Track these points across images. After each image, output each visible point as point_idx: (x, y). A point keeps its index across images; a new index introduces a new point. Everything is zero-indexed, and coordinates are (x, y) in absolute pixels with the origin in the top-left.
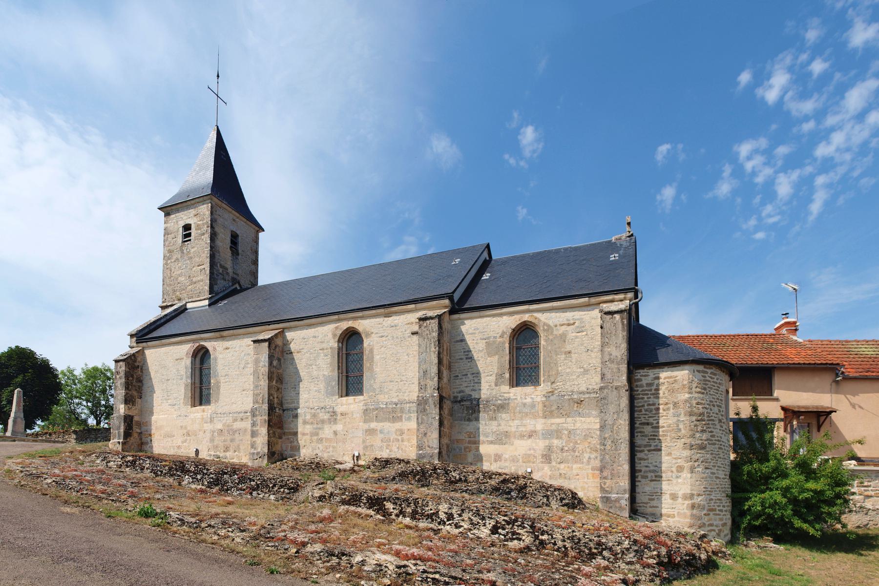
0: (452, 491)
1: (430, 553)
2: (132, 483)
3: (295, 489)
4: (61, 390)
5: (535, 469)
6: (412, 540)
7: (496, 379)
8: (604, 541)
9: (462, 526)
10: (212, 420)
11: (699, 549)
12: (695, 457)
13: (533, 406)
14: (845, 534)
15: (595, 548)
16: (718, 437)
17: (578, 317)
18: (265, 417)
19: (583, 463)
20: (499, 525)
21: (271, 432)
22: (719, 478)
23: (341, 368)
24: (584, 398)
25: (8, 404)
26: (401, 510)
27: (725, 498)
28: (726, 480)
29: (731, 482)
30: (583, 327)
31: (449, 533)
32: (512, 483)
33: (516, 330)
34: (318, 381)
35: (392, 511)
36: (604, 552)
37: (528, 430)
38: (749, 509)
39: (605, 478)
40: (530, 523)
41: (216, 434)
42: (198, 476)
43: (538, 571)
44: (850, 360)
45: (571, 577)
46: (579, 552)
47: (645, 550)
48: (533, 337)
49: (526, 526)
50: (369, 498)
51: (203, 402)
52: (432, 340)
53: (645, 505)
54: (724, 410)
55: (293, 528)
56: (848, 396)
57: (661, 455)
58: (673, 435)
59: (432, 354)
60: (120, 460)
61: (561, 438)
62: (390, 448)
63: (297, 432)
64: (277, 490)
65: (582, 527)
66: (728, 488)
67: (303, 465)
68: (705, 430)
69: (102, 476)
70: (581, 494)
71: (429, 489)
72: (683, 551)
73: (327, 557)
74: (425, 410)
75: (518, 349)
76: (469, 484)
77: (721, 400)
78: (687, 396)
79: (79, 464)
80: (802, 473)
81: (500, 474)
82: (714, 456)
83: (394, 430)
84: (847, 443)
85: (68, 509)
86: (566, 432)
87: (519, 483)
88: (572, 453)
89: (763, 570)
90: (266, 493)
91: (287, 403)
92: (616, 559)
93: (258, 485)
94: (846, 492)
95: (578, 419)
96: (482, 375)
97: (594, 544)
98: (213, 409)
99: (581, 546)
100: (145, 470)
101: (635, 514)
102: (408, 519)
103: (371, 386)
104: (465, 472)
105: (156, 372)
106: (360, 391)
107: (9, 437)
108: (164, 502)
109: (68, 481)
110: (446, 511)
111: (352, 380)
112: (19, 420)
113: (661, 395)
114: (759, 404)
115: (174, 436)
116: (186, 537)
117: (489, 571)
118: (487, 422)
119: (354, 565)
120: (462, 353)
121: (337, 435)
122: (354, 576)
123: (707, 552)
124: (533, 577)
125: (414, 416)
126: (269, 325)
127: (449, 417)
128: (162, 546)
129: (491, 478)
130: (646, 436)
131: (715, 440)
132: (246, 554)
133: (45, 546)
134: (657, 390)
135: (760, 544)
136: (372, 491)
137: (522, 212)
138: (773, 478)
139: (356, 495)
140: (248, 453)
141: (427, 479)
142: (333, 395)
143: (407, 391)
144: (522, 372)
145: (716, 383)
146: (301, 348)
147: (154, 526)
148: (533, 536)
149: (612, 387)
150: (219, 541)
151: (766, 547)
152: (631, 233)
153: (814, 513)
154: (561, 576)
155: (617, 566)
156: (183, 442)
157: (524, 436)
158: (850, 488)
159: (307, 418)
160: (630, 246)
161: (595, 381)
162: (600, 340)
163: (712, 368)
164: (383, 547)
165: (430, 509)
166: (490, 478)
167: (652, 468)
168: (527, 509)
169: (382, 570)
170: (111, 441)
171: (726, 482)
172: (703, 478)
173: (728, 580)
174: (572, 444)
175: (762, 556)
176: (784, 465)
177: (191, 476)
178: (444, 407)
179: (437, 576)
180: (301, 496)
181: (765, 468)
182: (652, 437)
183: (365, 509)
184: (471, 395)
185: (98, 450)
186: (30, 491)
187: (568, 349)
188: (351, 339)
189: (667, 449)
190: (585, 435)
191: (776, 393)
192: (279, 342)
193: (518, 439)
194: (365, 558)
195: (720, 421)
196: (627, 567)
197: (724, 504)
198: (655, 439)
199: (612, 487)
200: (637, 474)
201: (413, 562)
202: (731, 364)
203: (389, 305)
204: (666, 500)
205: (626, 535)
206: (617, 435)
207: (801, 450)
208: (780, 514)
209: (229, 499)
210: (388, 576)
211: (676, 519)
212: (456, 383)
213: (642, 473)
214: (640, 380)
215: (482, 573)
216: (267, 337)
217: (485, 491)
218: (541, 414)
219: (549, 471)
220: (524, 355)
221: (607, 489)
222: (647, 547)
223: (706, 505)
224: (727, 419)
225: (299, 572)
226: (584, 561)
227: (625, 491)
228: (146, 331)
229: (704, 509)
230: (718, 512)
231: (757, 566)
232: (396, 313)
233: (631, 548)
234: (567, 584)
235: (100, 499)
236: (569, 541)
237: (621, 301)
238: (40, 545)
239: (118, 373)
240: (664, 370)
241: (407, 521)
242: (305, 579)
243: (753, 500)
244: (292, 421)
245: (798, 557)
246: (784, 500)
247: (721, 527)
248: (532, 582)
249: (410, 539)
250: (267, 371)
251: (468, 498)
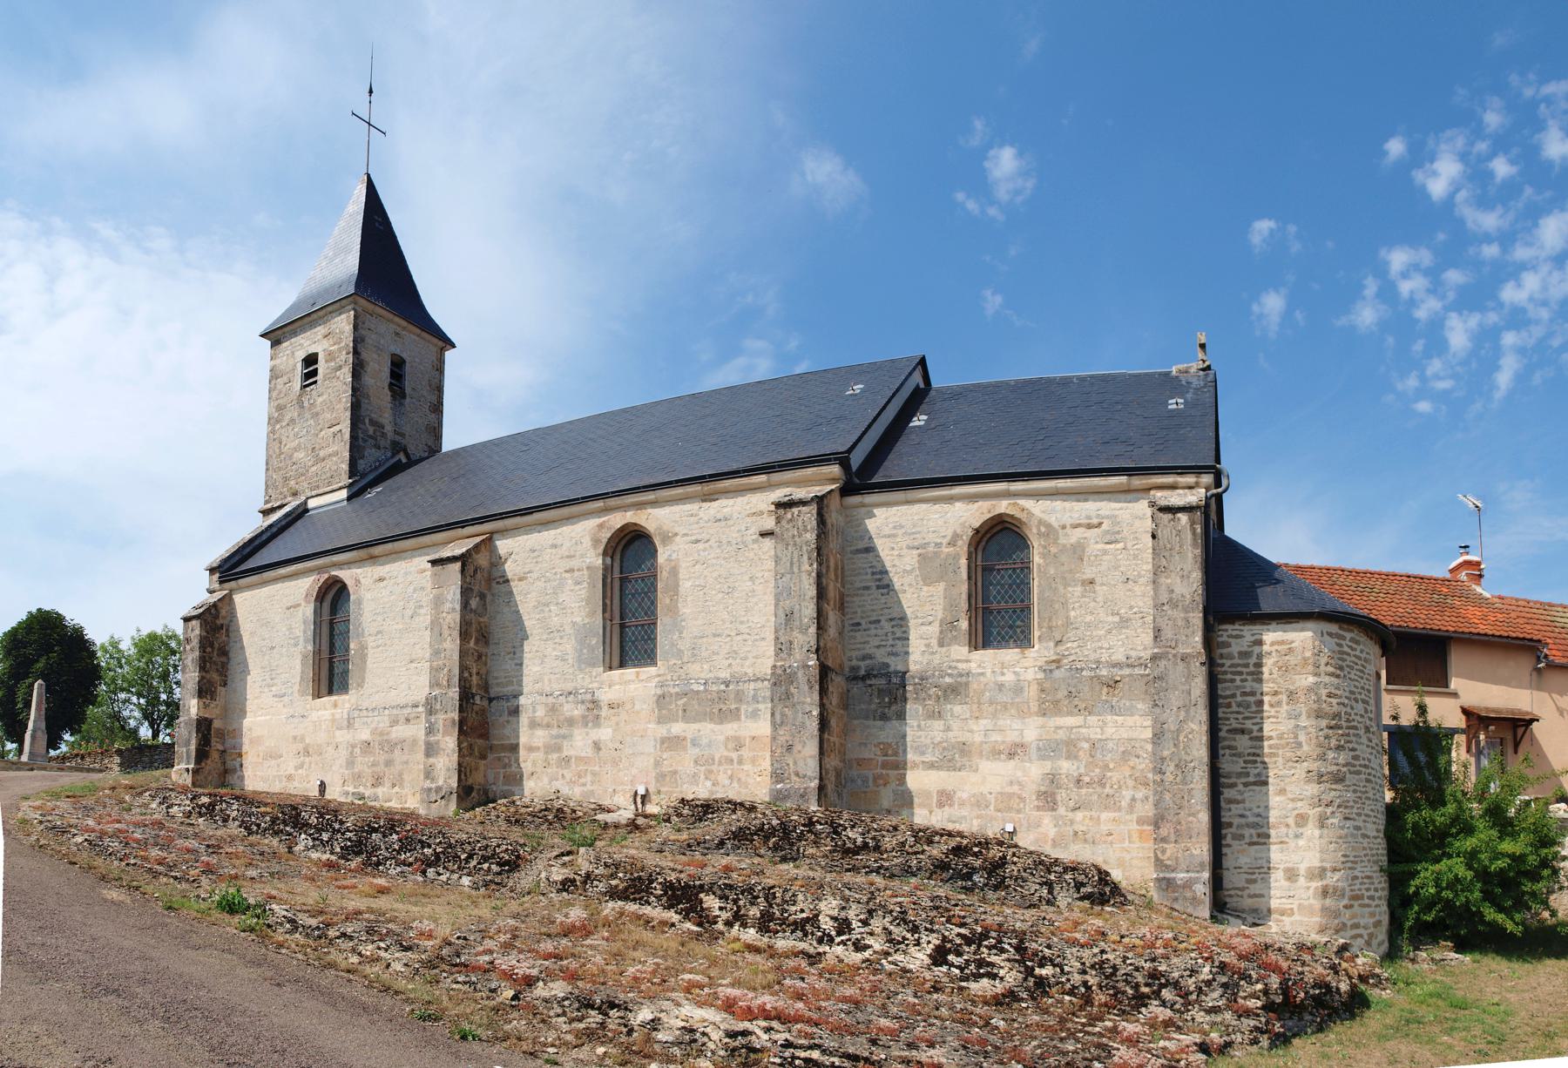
0: (848, 870)
1: (800, 1005)
2: (208, 846)
3: (513, 865)
4: (100, 678)
5: (1021, 825)
6: (760, 976)
7: (941, 632)
8: (1162, 968)
9: (870, 947)
10: (350, 724)
11: (1336, 973)
12: (1327, 797)
13: (1018, 689)
14: (1556, 926)
15: (1147, 985)
16: (1364, 759)
17: (1108, 513)
18: (453, 715)
19: (1120, 809)
20: (949, 945)
21: (465, 744)
22: (1368, 837)
23: (609, 608)
24: (1121, 676)
25: (24, 707)
26: (737, 913)
27: (1378, 874)
28: (1379, 840)
29: (1388, 844)
30: (1118, 533)
31: (841, 961)
32: (976, 855)
33: (983, 531)
34: (561, 638)
35: (717, 913)
36: (1164, 990)
37: (1008, 739)
38: (1416, 893)
39: (1164, 840)
40: (1014, 941)
41: (357, 750)
42: (324, 834)
43: (1031, 1037)
44: (1555, 635)
45: (1099, 1046)
46: (1115, 995)
47: (1242, 983)
48: (1018, 547)
49: (1007, 946)
50: (668, 886)
51: (335, 687)
52: (805, 548)
53: (1240, 893)
54: (1373, 709)
55: (507, 947)
56: (1554, 695)
57: (1267, 794)
58: (1288, 754)
59: (804, 576)
60: (188, 802)
61: (1076, 757)
62: (713, 777)
63: (518, 745)
64: (475, 867)
65: (1120, 942)
66: (1383, 855)
67: (529, 815)
68: (1342, 747)
69: (161, 833)
70: (1116, 875)
71: (797, 867)
72: (1309, 979)
73: (578, 1010)
74: (788, 695)
75: (987, 570)
76: (885, 856)
77: (1369, 691)
78: (1311, 679)
79: (124, 809)
80: (1494, 825)
81: (950, 834)
82: (1359, 794)
83: (722, 738)
84: (1555, 775)
85: (113, 894)
86: (1086, 745)
87: (990, 855)
88: (1099, 789)
89: (1440, 1002)
90: (453, 872)
91: (498, 684)
92: (1187, 1004)
93: (437, 855)
94: (1556, 856)
95: (1109, 718)
96: (912, 623)
97: (1144, 976)
98: (353, 700)
99: (1117, 981)
100: (230, 822)
101: (1222, 912)
102: (752, 931)
103: (673, 645)
104: (876, 830)
105: (252, 634)
106: (649, 657)
107: (25, 764)
108: (263, 885)
109: (107, 840)
110: (835, 913)
111: (633, 633)
112: (39, 734)
113: (1266, 676)
114: (1430, 701)
115: (281, 757)
116: (300, 956)
117: (931, 1045)
118: (923, 723)
119: (636, 1028)
120: (869, 577)
121: (600, 749)
122: (636, 1053)
123: (1350, 978)
124: (1021, 1051)
125: (765, 708)
126: (463, 527)
127: (842, 712)
128: (269, 974)
129: (932, 842)
130: (1240, 755)
131: (1360, 766)
132: (412, 996)
133: (73, 963)
134: (1259, 665)
135: (1434, 956)
136: (673, 870)
137: (993, 301)
138: (1452, 835)
139: (640, 878)
140: (418, 789)
141: (792, 844)
142: (594, 665)
143: (750, 655)
144: (995, 618)
145: (1360, 658)
146: (527, 570)
147: (244, 931)
148: (1022, 969)
149: (1174, 656)
150: (360, 967)
151: (1443, 960)
152: (1207, 363)
153: (1512, 894)
154: (1080, 1046)
155: (1189, 1018)
156: (297, 768)
157: (1000, 753)
158: (1559, 849)
159: (537, 714)
160: (1205, 386)
161: (1140, 643)
162: (1151, 560)
163: (1352, 631)
164: (698, 991)
165: (801, 908)
166: (930, 842)
167: (1251, 819)
168: (1008, 911)
169: (695, 1041)
170: (176, 767)
171: (1380, 844)
172: (1341, 838)
173: (1386, 1027)
174: (1097, 770)
175: (1438, 978)
176: (1468, 812)
177: (310, 835)
178: (831, 689)
179: (815, 1055)
180: (525, 879)
181: (1441, 817)
182: (1251, 758)
183: (659, 909)
184: (887, 665)
185: (154, 785)
186: (52, 856)
187: (1088, 575)
188: (632, 547)
189: (1278, 781)
190: (1124, 752)
191: (1455, 683)
192: (482, 560)
193: (988, 759)
194: (658, 1015)
195: (1367, 729)
196: (1208, 1018)
197: (1376, 886)
198: (1256, 762)
199: (1177, 858)
200: (1224, 832)
201: (764, 1024)
202: (1383, 625)
203: (711, 476)
204: (1278, 881)
205: (1206, 955)
206: (1186, 753)
207: (1492, 785)
208: (1464, 899)
209: (381, 881)
210: (709, 1054)
211: (1297, 917)
212: (855, 638)
213: (1233, 830)
214: (1228, 645)
215: (917, 1048)
216: (458, 552)
217: (919, 869)
218: (1034, 708)
219: (1051, 825)
220: (998, 583)
221: (1169, 863)
222: (1245, 976)
223: (1348, 889)
224: (1378, 726)
225: (519, 1039)
226: (1124, 1011)
227: (1202, 864)
228: (237, 558)
229: (1343, 896)
230: (1366, 901)
231: (1431, 995)
232: (726, 493)
233: (1214, 980)
234: (1091, 1061)
235: (156, 875)
236: (1094, 973)
237: (1190, 488)
238: (65, 960)
239: (188, 640)
240: (1269, 627)
241: (751, 935)
242: (531, 1054)
243: (1422, 875)
244: (508, 722)
245: (1491, 972)
246: (1470, 874)
247: (1372, 929)
248: (1018, 1062)
249: (756, 974)
250: (458, 620)
251: (881, 886)
